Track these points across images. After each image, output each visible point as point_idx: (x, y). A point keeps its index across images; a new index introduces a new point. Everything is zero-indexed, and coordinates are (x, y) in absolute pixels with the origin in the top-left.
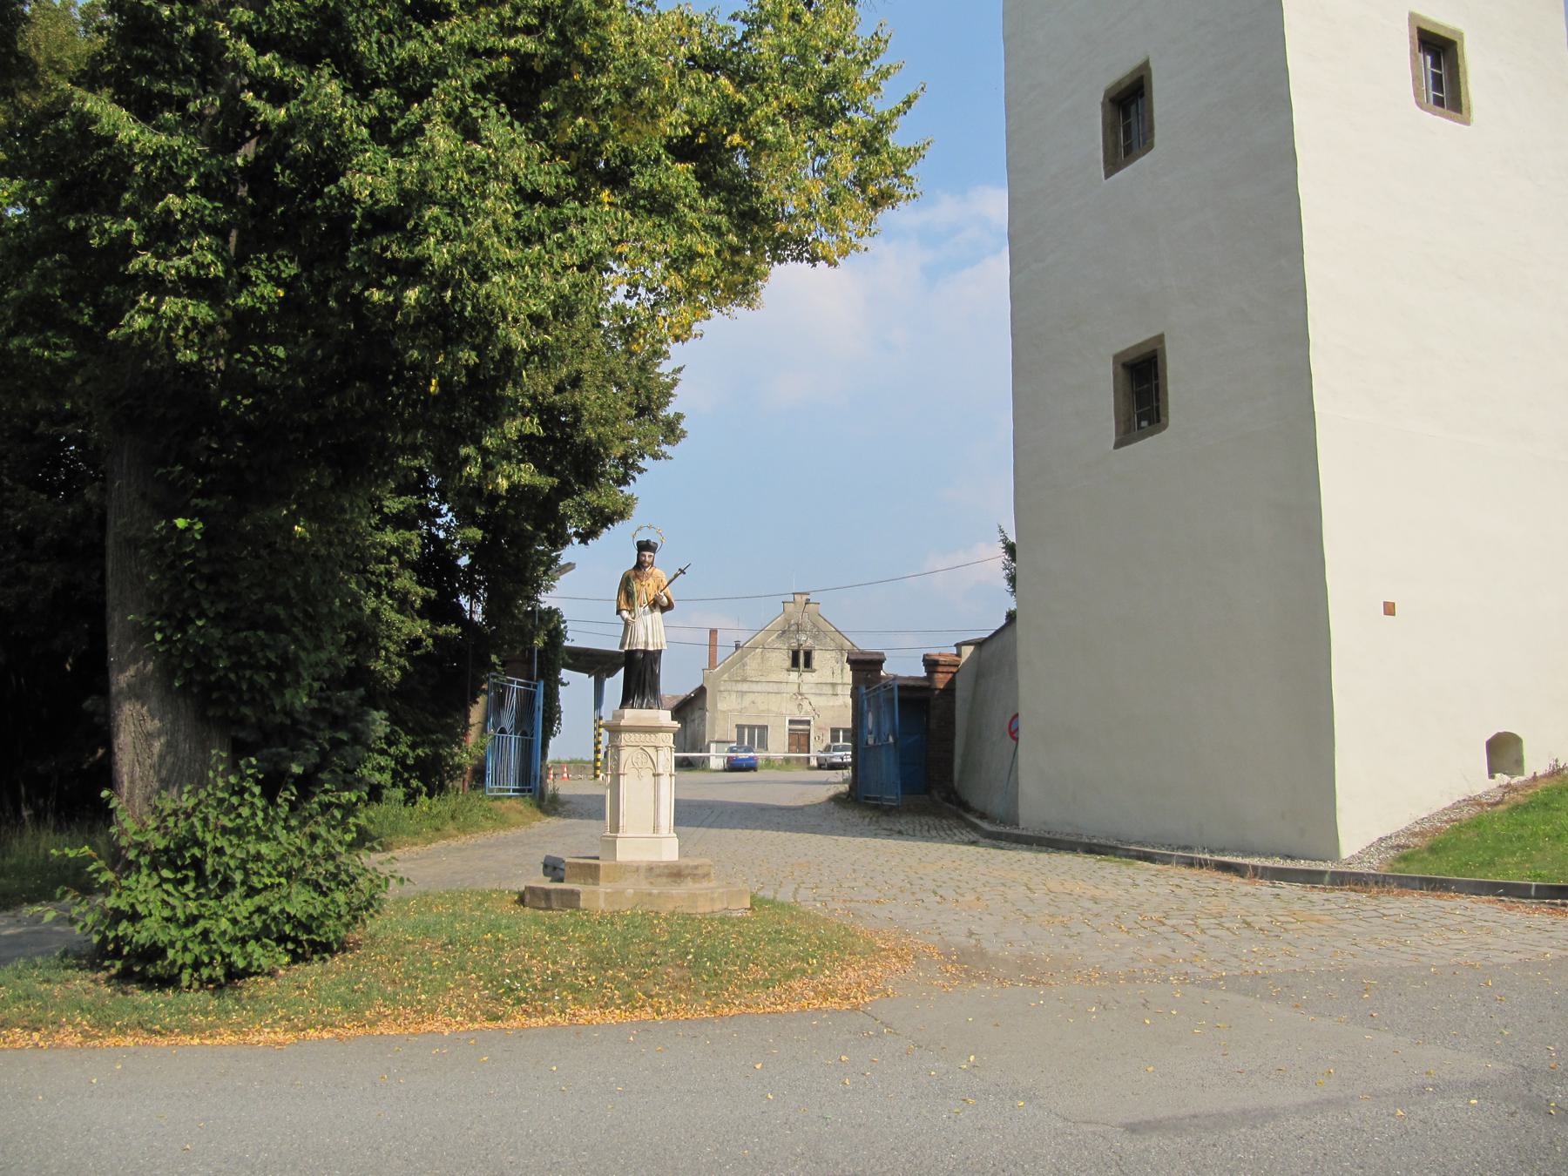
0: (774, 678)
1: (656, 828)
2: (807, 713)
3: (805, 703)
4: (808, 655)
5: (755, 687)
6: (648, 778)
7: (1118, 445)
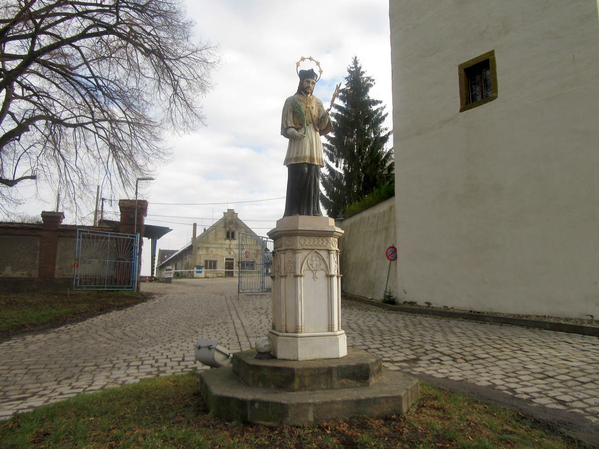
0: (220, 242)
1: (330, 328)
2: (232, 256)
3: (232, 252)
4: (233, 234)
5: (212, 246)
6: (321, 274)
7: (461, 111)
